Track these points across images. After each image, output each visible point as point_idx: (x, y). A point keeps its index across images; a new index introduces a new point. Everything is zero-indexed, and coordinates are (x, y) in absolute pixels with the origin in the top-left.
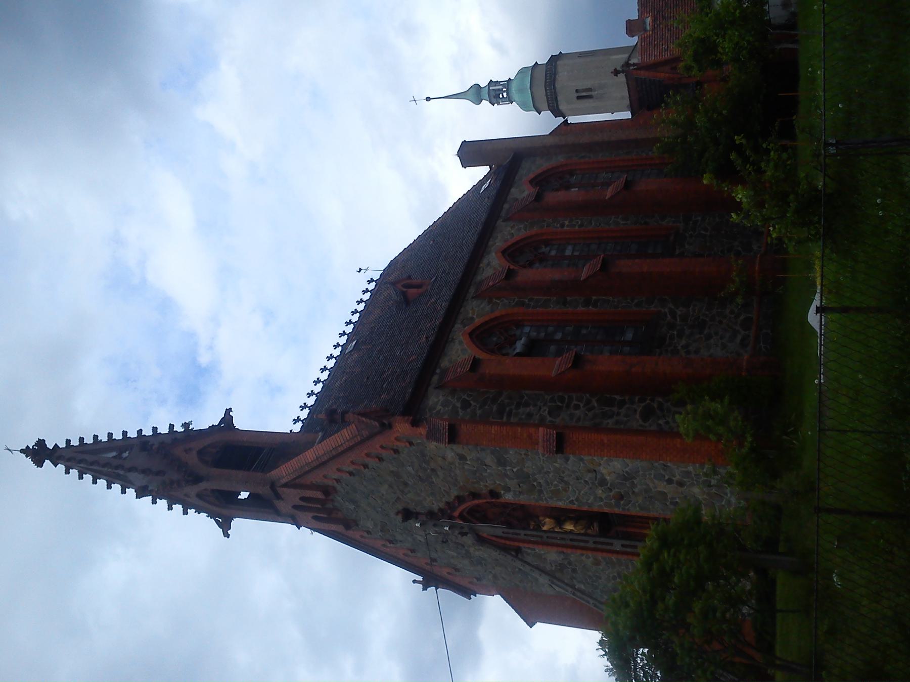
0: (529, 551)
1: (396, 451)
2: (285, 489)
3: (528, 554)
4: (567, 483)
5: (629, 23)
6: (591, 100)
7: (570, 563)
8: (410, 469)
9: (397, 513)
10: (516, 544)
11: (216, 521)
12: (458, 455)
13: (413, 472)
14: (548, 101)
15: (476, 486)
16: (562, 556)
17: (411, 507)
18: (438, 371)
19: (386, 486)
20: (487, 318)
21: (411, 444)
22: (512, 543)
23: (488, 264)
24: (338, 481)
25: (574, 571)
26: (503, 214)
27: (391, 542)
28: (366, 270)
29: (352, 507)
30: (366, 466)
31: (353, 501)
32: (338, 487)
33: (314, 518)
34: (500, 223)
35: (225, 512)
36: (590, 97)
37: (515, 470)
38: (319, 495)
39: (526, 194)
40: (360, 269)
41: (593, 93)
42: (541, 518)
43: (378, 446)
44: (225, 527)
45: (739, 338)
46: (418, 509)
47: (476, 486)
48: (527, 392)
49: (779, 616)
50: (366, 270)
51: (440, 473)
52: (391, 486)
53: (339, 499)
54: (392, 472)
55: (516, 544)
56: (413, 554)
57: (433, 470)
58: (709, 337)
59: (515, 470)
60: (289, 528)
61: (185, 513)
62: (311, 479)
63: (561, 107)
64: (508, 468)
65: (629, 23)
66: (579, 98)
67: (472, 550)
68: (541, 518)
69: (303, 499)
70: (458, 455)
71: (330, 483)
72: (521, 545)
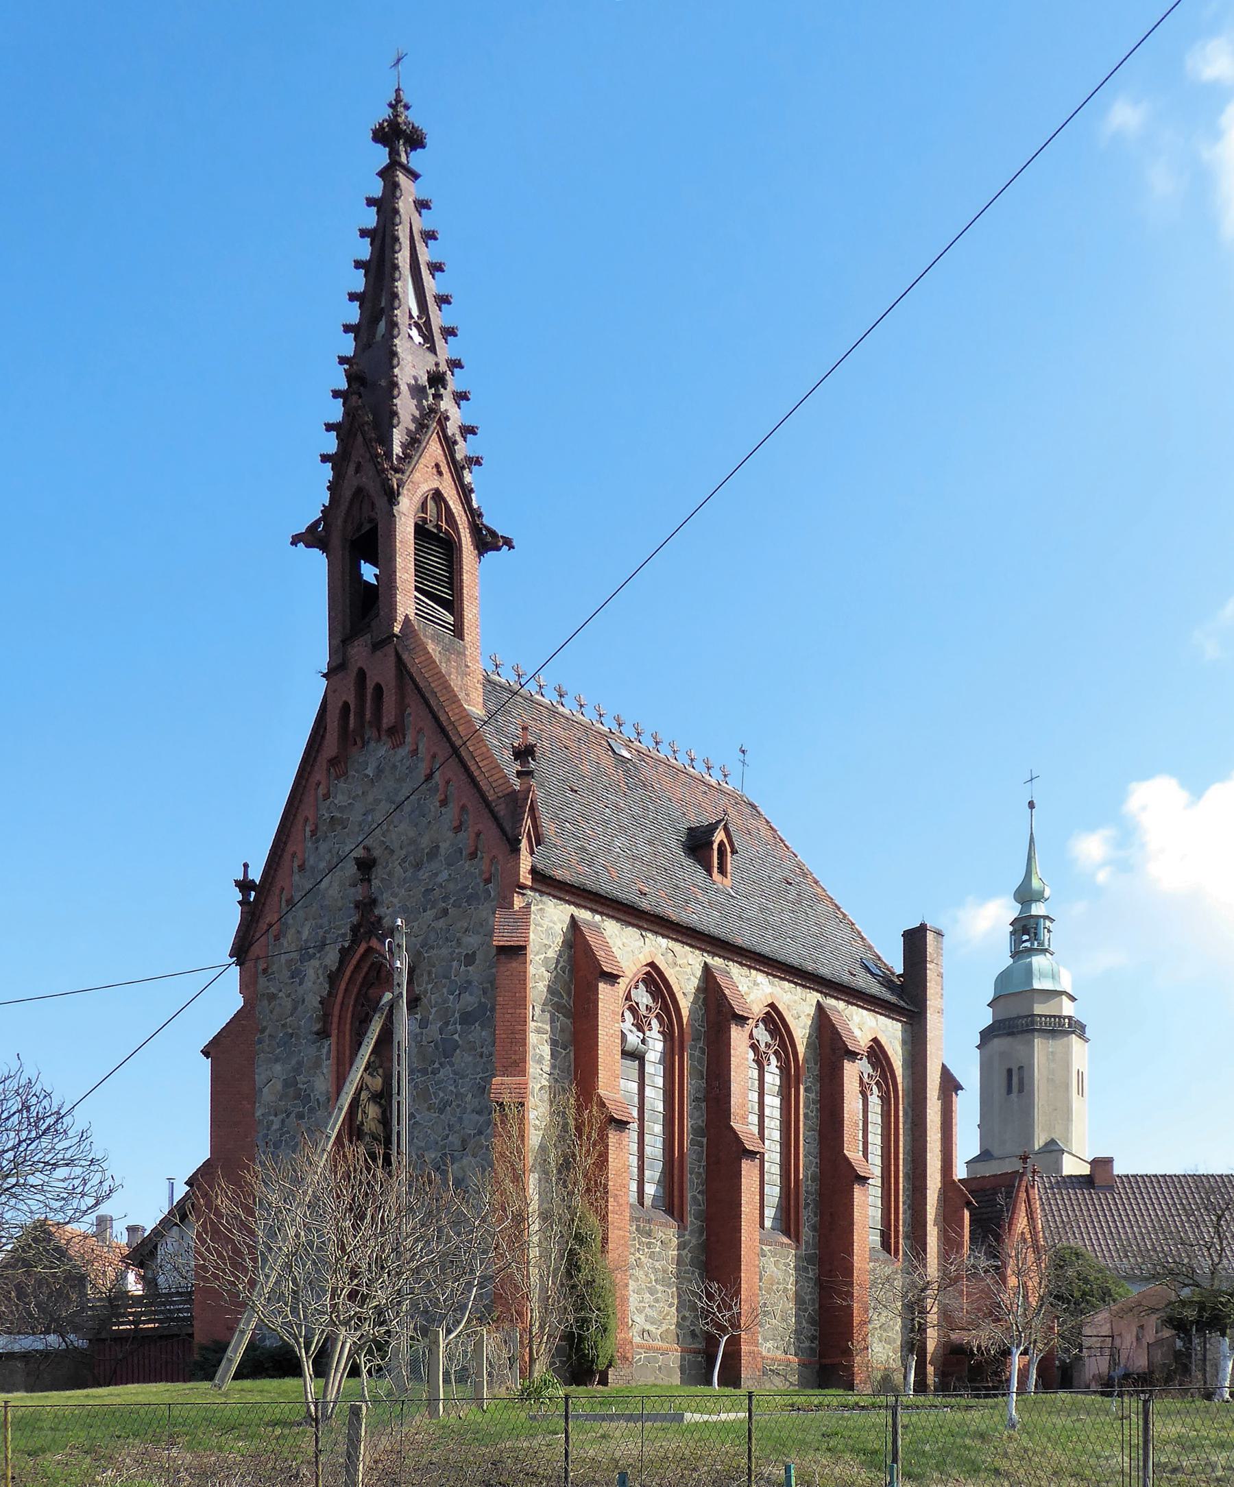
0: (325, 1051)
1: (473, 856)
2: (392, 659)
3: (319, 1049)
4: (441, 1111)
5: (1108, 1162)
6: (1004, 1090)
7: (311, 1110)
8: (445, 875)
9: (367, 849)
10: (335, 1032)
11: (317, 523)
12: (474, 953)
13: (439, 879)
14: (1010, 1019)
15: (425, 977)
16: (322, 1099)
17: (379, 873)
18: (598, 918)
19: (412, 834)
20: (675, 988)
21: (488, 881)
22: (334, 1026)
23: (756, 984)
24: (415, 752)
25: (300, 1116)
26: (831, 1002)
27: (313, 833)
28: (744, 763)
29: (370, 772)
30: (444, 803)
31: (379, 771)
32: (403, 752)
33: (346, 707)
34: (814, 997)
35: (336, 541)
36: (1009, 1091)
37: (456, 1037)
38: (388, 720)
39: (857, 1033)
40: (743, 752)
41: (1014, 1095)
42: (381, 1071)
43: (480, 827)
44: (311, 537)
45: (652, 1328)
46: (376, 883)
47: (425, 977)
48: (572, 1054)
49: (1132, 1404)
50: (744, 763)
51: (441, 923)
52: (413, 842)
53: (382, 752)
54: (437, 847)
55: (335, 1032)
56: (296, 869)
57: (445, 912)
58: (652, 1292)
59: (456, 1037)
60: (321, 658)
61: (325, 458)
62: (414, 710)
63: (996, 1041)
64: (459, 1027)
65: (1108, 1162)
66: (1010, 1071)
67: (315, 963)
68: (381, 1071)
69: (379, 689)
70: (474, 953)
71: (409, 739)
72: (333, 1039)
